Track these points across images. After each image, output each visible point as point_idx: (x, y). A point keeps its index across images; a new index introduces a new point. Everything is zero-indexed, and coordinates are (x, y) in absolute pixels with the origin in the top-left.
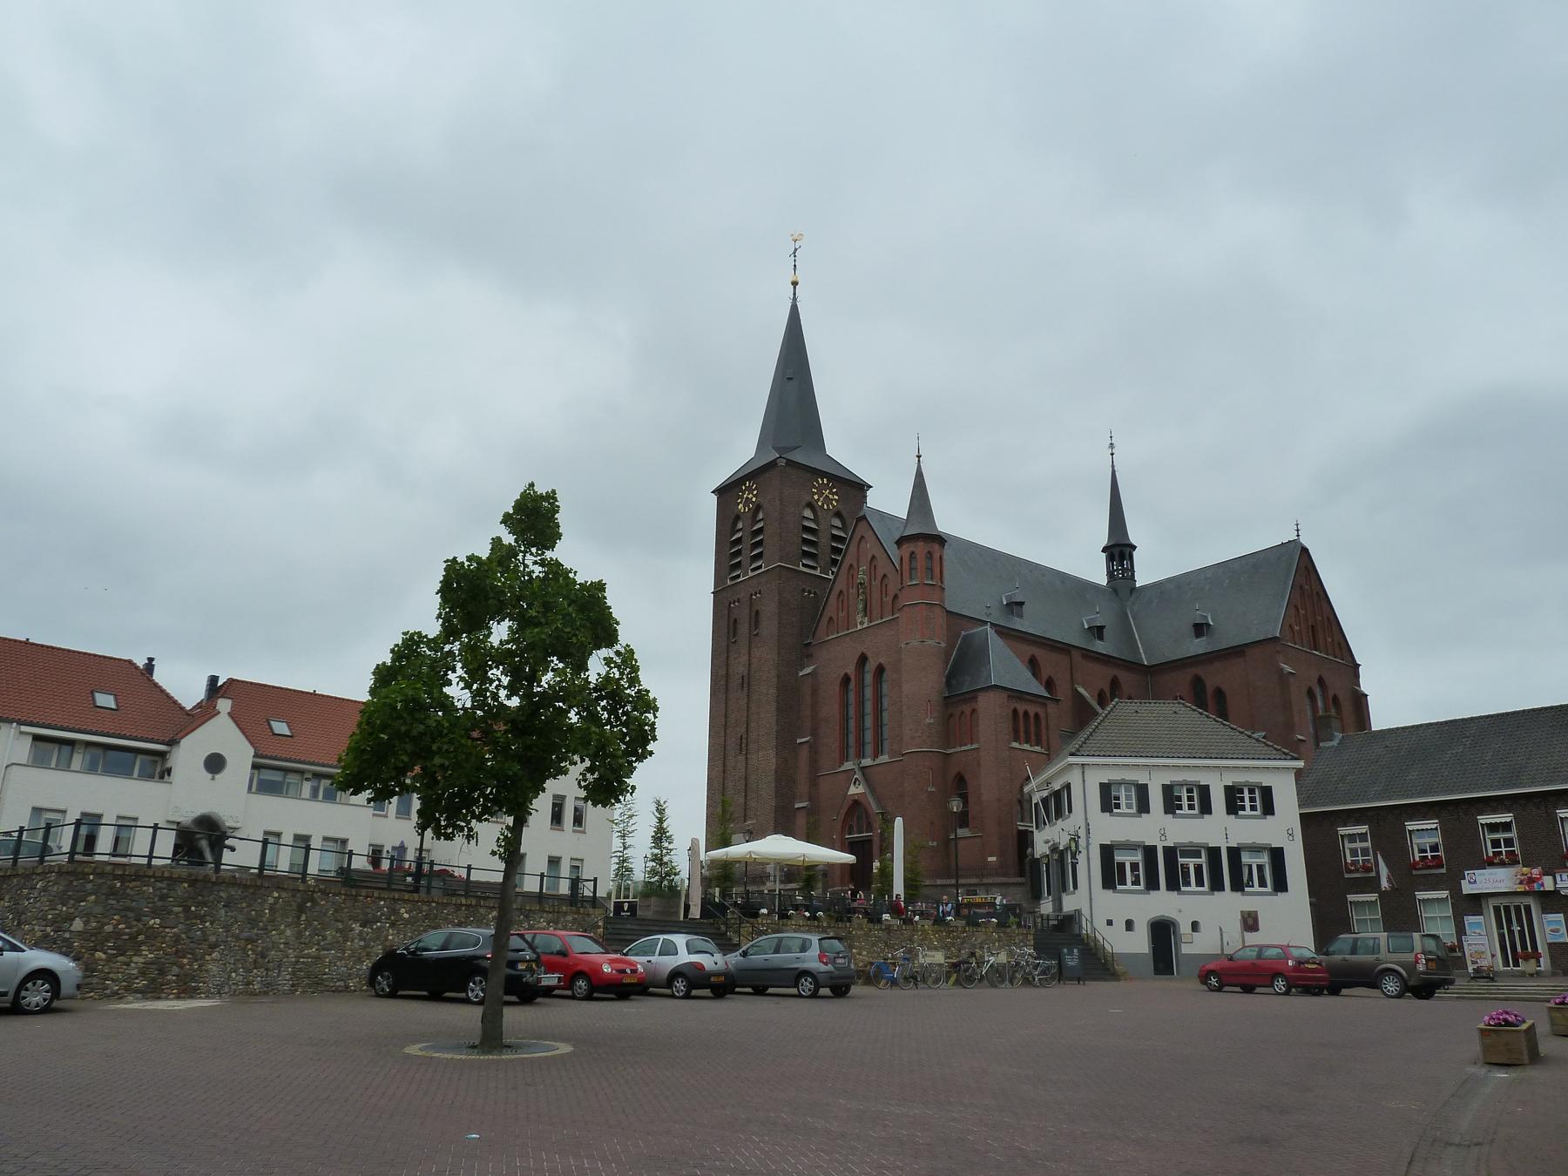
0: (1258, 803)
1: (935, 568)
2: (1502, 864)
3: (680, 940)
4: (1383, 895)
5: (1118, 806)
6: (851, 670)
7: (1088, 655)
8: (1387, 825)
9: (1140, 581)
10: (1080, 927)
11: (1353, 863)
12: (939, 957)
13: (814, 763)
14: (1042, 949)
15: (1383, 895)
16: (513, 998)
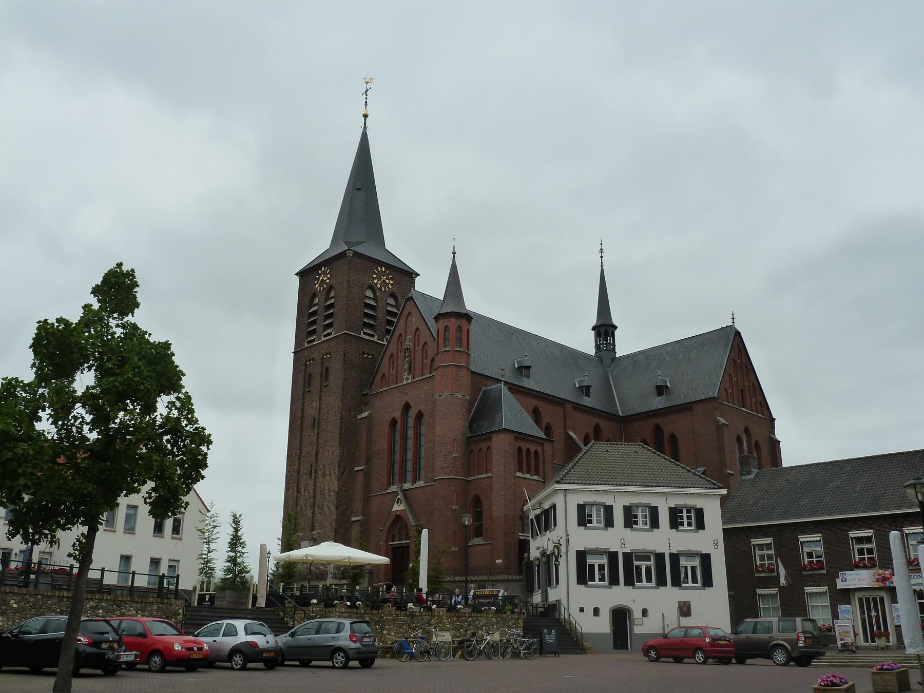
0: (693, 521)
1: (463, 338)
2: (865, 567)
3: (240, 624)
4: (782, 590)
5: (590, 522)
6: (398, 415)
7: (578, 407)
8: (786, 537)
9: (621, 351)
10: (560, 613)
11: (762, 566)
12: (447, 637)
13: (367, 487)
14: (528, 630)
15: (782, 590)
16: (99, 672)
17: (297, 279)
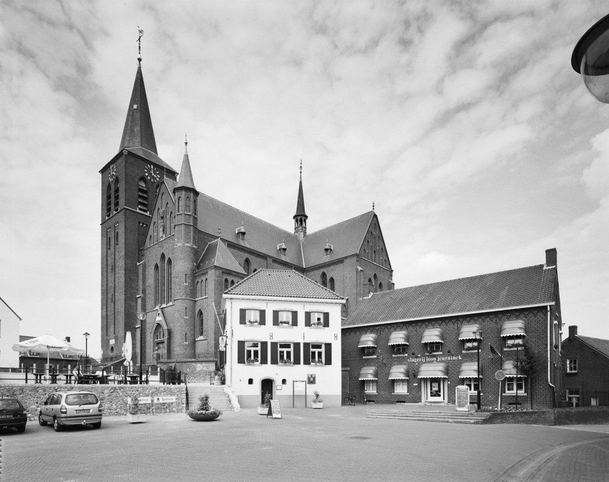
17: (100, 175)
